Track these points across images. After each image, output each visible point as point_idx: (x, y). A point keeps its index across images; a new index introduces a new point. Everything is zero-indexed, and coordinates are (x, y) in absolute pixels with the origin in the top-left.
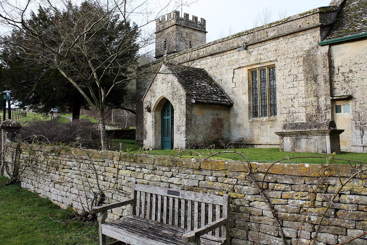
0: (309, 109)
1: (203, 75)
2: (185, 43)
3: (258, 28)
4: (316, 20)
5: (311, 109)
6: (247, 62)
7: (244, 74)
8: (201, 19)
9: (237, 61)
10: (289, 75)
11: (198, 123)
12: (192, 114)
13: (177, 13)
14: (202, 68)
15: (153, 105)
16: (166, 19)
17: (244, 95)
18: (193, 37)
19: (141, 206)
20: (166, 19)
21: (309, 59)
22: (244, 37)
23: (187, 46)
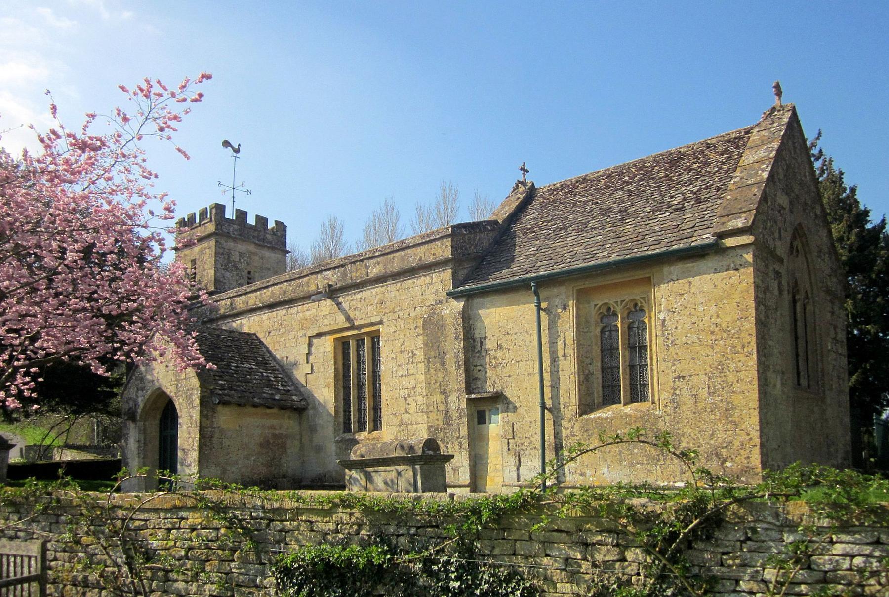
0: (433, 416)
1: (250, 345)
2: (237, 275)
3: (353, 256)
4: (444, 250)
5: (436, 417)
6: (332, 322)
7: (326, 347)
8: (277, 223)
9: (314, 320)
10: (401, 352)
11: (227, 443)
12: (215, 426)
13: (220, 209)
14: (253, 331)
15: (141, 406)
16: (197, 221)
17: (327, 389)
18: (256, 261)
19: (15, 567)
20: (197, 221)
21: (432, 326)
22: (328, 272)
23: (242, 281)
